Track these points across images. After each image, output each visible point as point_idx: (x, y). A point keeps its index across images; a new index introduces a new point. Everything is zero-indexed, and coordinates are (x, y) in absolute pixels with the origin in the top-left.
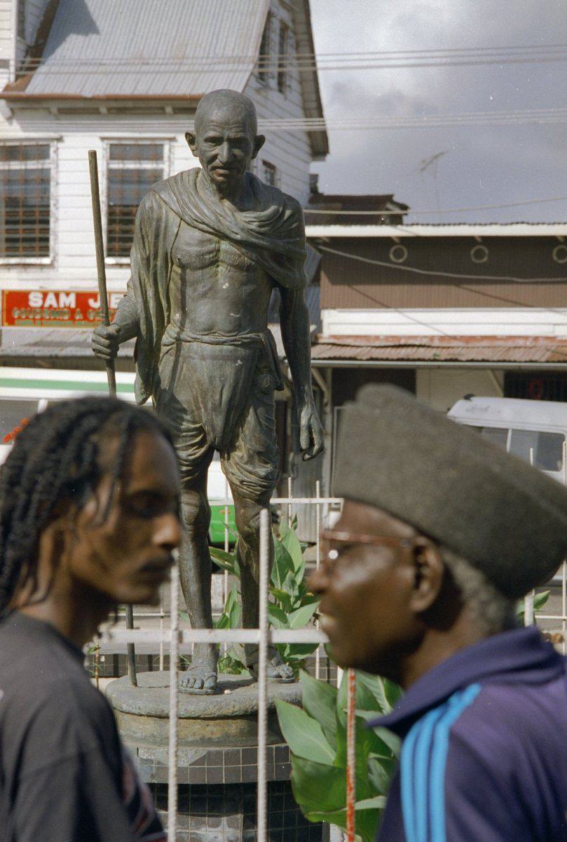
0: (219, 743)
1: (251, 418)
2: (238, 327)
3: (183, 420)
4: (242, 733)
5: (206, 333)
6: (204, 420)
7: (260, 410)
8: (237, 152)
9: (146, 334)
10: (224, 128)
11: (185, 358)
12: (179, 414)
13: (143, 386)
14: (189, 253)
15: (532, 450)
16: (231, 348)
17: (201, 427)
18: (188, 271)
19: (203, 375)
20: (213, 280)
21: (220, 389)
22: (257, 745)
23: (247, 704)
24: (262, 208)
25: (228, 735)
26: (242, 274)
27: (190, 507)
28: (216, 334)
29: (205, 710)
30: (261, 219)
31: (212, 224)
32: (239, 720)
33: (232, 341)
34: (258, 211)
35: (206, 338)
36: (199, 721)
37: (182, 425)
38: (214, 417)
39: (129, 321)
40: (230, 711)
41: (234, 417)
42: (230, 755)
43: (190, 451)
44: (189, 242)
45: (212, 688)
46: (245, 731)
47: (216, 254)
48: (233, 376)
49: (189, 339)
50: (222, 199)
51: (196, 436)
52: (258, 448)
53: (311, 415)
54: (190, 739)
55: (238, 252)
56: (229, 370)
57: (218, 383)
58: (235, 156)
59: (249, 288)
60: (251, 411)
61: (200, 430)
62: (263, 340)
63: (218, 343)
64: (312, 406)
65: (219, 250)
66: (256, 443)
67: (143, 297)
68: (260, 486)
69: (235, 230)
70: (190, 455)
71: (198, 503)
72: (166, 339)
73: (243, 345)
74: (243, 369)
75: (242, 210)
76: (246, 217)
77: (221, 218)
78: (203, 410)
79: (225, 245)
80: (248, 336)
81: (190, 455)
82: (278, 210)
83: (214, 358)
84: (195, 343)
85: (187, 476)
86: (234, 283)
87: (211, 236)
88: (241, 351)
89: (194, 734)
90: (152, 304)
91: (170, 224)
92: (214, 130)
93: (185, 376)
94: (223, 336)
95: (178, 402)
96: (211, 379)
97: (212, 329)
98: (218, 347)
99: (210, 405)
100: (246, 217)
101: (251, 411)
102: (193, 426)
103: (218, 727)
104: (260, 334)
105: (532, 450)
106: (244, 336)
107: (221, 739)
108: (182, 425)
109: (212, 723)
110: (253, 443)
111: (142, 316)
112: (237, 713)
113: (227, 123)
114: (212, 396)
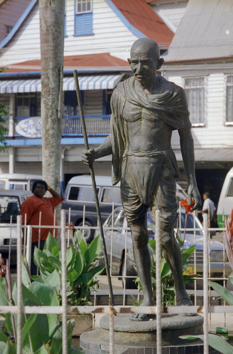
0: (137, 344)
1: (159, 191)
2: (151, 148)
3: (129, 192)
4: (148, 340)
5: (136, 152)
6: (138, 192)
7: (164, 187)
8: (146, 67)
9: (115, 153)
10: (138, 56)
11: (129, 163)
12: (127, 190)
13: (115, 177)
14: (128, 115)
15: (26, 214)
16: (148, 158)
17: (137, 195)
18: (128, 123)
19: (135, 171)
20: (139, 127)
21: (142, 177)
22: (156, 346)
23: (150, 326)
24: (162, 92)
25: (141, 341)
26: (152, 124)
27: (136, 232)
28: (141, 152)
29: (130, 329)
30: (159, 98)
31: (136, 101)
32: (147, 334)
33: (148, 155)
34: (160, 94)
35: (136, 154)
36: (129, 333)
37: (129, 194)
38: (141, 190)
39: (106, 147)
40: (143, 329)
41: (151, 189)
42: (139, 350)
43: (133, 207)
44: (129, 111)
45: (141, 318)
46: (150, 339)
47: (140, 115)
48: (148, 172)
49: (130, 155)
50: (144, 89)
51: (135, 200)
52: (163, 205)
53: (193, 189)
54: (125, 342)
55: (149, 113)
56: (147, 169)
57: (142, 175)
58: (144, 69)
59: (154, 131)
60: (159, 187)
61: (137, 197)
62: (165, 154)
63: (141, 156)
64: (194, 185)
65: (141, 113)
66: (162, 202)
67: (114, 136)
68: (165, 223)
69: (147, 104)
70: (133, 209)
71: (139, 231)
72: (124, 155)
73: (153, 157)
74: (154, 168)
75: (152, 94)
76: (152, 97)
77: (141, 98)
78: (137, 187)
79: (144, 111)
80: (156, 152)
81: (133, 209)
82: (169, 93)
83: (140, 163)
84: (132, 156)
85: (133, 218)
86: (148, 128)
87: (138, 107)
88: (153, 160)
89: (127, 339)
90: (118, 139)
91: (122, 102)
92: (134, 57)
93: (129, 172)
94: (144, 153)
95: (127, 184)
96: (138, 173)
97: (139, 150)
98: (141, 158)
99: (139, 186)
100: (152, 97)
101: (159, 187)
102: (133, 195)
103: (137, 337)
104: (164, 152)
105: (26, 214)
106: (154, 153)
107: (139, 342)
108: (129, 194)
109: (134, 334)
110: (161, 203)
111: (113, 144)
112: (146, 330)
113: (139, 53)
114: (139, 181)
